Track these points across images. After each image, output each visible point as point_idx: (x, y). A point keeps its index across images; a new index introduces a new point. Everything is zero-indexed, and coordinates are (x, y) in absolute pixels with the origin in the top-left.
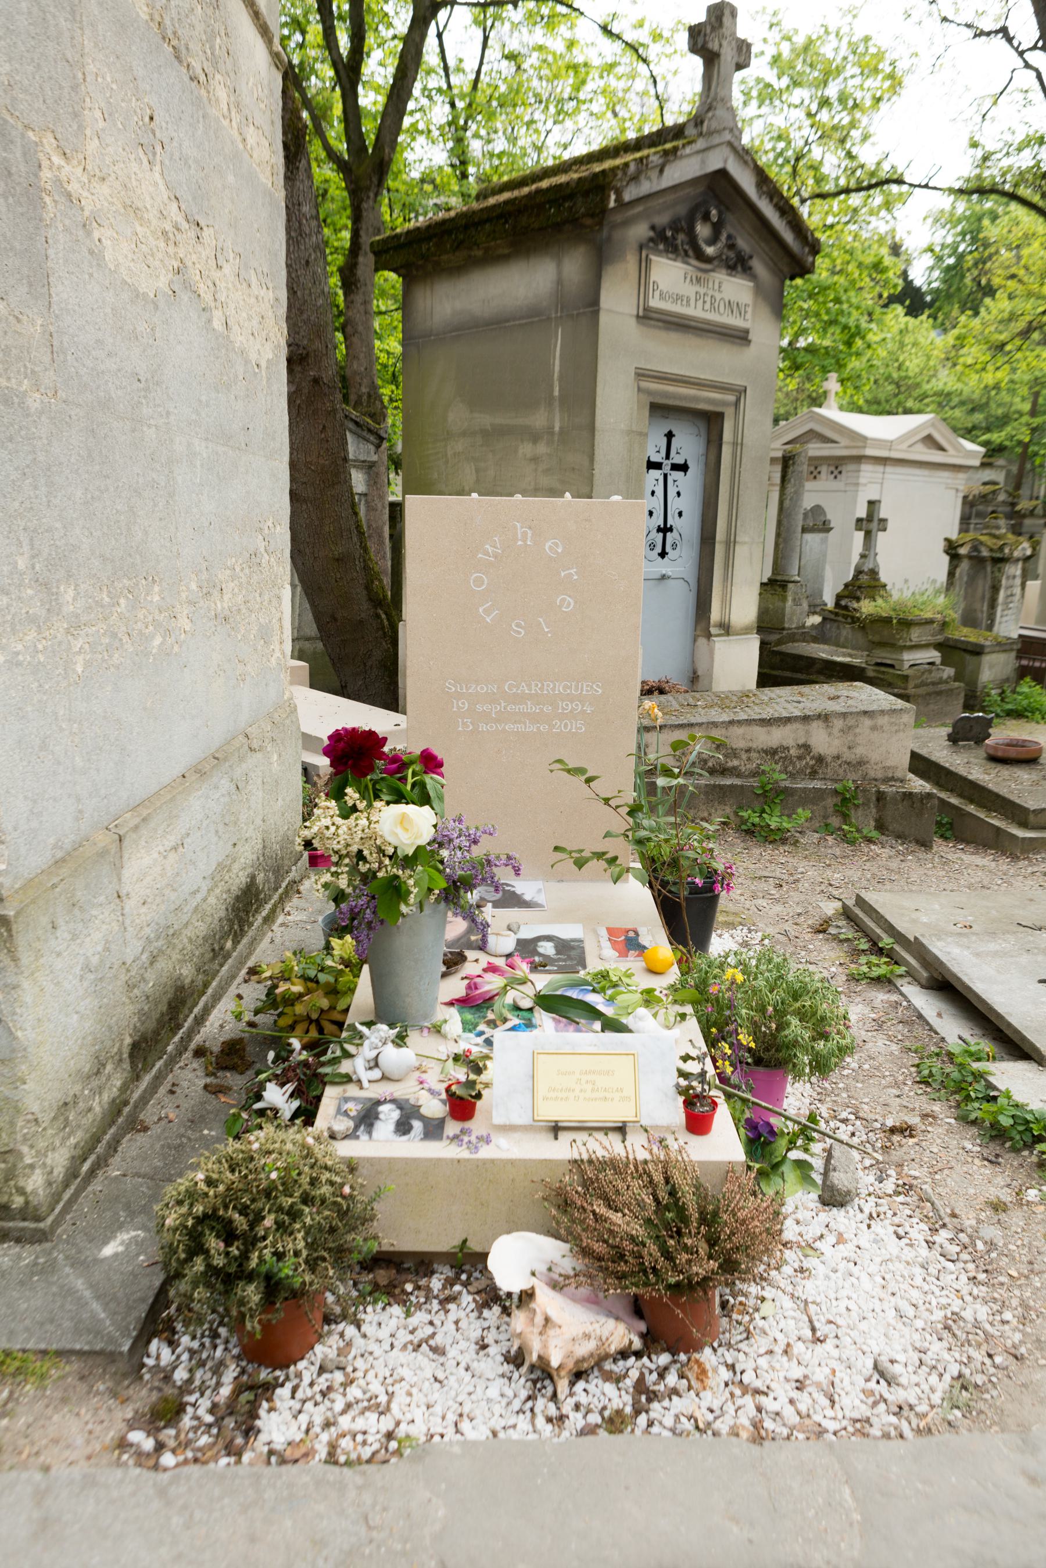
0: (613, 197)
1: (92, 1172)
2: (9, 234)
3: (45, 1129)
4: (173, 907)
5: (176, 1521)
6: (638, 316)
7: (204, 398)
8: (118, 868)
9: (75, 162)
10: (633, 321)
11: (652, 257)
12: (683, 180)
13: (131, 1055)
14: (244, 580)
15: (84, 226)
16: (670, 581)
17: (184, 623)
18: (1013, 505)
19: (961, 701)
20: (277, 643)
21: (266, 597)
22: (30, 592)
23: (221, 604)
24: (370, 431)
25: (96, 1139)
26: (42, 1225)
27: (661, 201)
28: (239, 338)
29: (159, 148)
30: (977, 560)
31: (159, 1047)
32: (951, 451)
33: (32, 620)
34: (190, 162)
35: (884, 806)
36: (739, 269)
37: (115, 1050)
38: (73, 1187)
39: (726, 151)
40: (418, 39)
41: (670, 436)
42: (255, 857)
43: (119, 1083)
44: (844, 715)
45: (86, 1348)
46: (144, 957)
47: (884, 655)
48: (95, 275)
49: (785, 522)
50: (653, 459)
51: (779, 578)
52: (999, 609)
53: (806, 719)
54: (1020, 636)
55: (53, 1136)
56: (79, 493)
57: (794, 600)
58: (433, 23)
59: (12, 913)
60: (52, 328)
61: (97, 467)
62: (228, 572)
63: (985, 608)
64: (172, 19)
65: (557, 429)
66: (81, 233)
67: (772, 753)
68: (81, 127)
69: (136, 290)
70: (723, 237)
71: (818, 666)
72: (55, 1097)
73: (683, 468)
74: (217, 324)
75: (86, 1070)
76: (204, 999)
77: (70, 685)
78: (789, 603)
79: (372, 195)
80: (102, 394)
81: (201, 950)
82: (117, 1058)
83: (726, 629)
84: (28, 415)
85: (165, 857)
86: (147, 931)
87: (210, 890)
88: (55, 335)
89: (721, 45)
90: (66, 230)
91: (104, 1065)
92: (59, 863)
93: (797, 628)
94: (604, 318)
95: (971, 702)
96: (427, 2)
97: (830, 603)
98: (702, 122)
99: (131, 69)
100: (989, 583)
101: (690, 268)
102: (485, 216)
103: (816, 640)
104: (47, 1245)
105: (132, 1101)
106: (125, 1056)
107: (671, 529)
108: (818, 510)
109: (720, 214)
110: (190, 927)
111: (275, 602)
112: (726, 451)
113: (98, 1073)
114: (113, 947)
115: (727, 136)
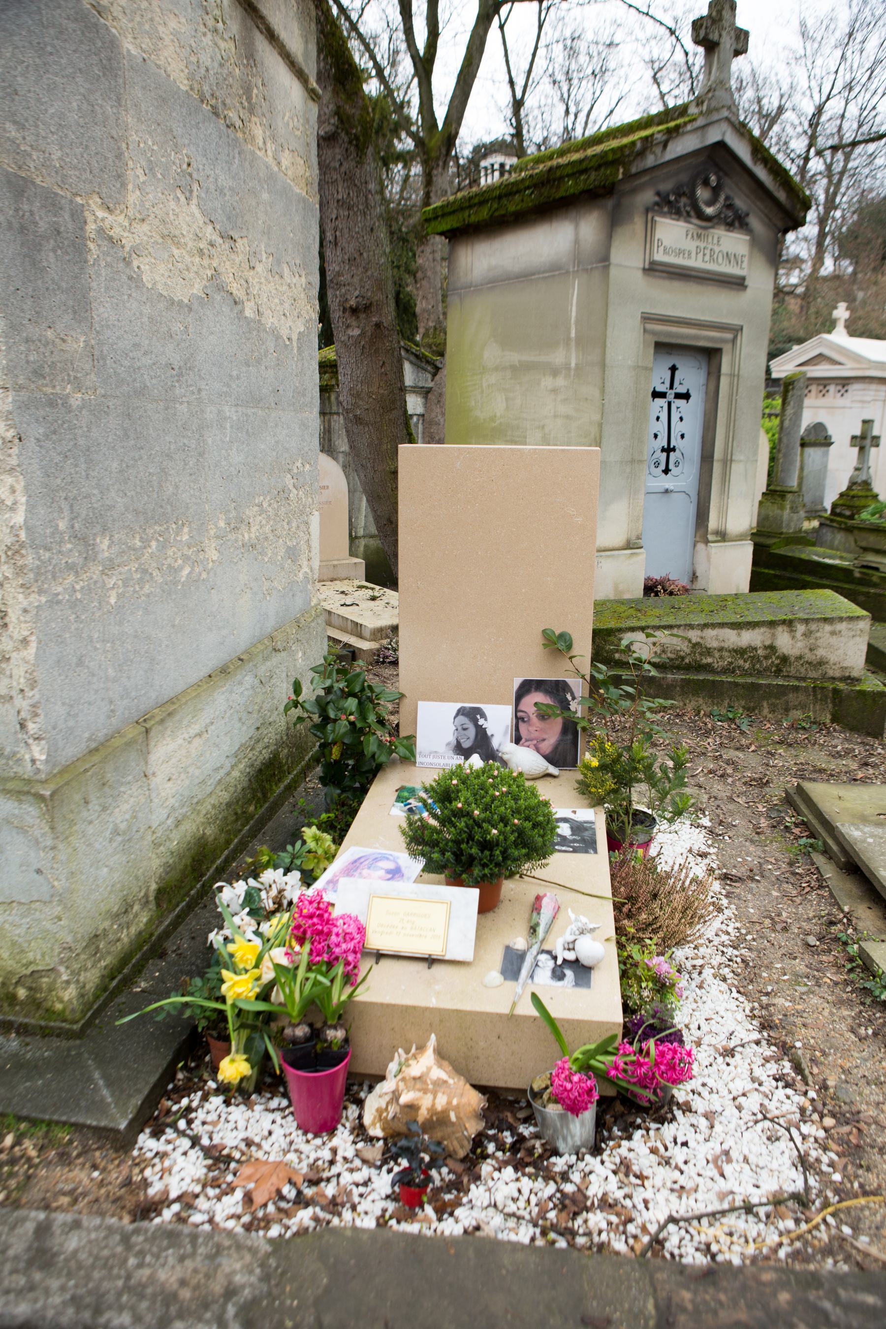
0: (621, 170)
2: (56, 278)
3: (78, 955)
4: (197, 781)
6: (644, 269)
7: (234, 373)
8: (145, 753)
10: (640, 273)
11: (657, 219)
12: (685, 152)
13: (157, 898)
14: (271, 512)
16: (673, 494)
20: (305, 563)
21: (294, 524)
22: (69, 546)
24: (428, 362)
26: (75, 1027)
27: (665, 171)
33: (70, 567)
34: (226, 191)
36: (737, 224)
37: (142, 894)
39: (724, 126)
40: (482, 33)
41: (673, 369)
42: (278, 737)
44: (806, 621)
46: (169, 822)
48: (134, 295)
53: (772, 624)
55: (85, 960)
56: (115, 464)
57: (792, 508)
58: (496, 17)
60: (93, 342)
61: (133, 442)
62: (256, 508)
64: (211, 85)
65: (573, 365)
67: (740, 652)
68: (124, 185)
70: (722, 198)
73: (686, 396)
75: (115, 910)
77: (104, 614)
79: (441, 163)
81: (225, 814)
82: (144, 900)
83: (722, 536)
84: (70, 412)
85: (189, 742)
86: (172, 801)
87: (232, 767)
89: (720, 36)
90: (108, 265)
91: (132, 907)
93: (795, 532)
94: (613, 271)
96: (491, 2)
98: (702, 102)
99: (171, 131)
101: (691, 226)
102: (515, 189)
106: (151, 898)
107: (674, 450)
108: (819, 428)
109: (719, 179)
110: (214, 796)
111: (303, 528)
112: (724, 382)
113: (126, 912)
114: (140, 815)
115: (725, 113)
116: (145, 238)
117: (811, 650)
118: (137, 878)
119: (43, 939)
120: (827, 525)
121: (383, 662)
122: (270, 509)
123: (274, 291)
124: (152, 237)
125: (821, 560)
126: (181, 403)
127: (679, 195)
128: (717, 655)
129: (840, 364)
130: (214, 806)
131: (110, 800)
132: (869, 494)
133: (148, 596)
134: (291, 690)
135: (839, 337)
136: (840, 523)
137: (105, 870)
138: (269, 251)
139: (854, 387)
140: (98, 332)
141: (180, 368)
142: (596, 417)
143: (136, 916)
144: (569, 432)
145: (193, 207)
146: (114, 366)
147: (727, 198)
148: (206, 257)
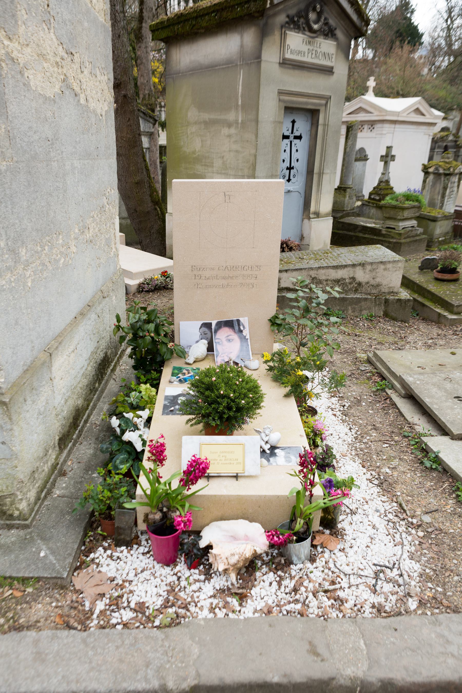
1: (45, 497)
5: (91, 653)
6: (280, 63)
7: (78, 140)
8: (50, 367)
9: (14, 40)
10: (277, 66)
11: (287, 32)
15: (21, 72)
16: (292, 193)
17: (74, 249)
18: (456, 141)
19: (425, 244)
22: (7, 256)
23: (88, 235)
25: (46, 482)
26: (26, 522)
28: (92, 105)
29: (52, 20)
30: (437, 175)
31: (70, 437)
32: (428, 116)
34: (67, 22)
35: (388, 305)
36: (330, 35)
38: (38, 504)
41: (293, 122)
43: (54, 457)
44: (372, 264)
45: (49, 576)
47: (391, 223)
48: (27, 95)
49: (347, 159)
50: (285, 134)
51: (343, 186)
52: (446, 198)
53: (354, 266)
54: (455, 210)
55: (29, 486)
56: (25, 204)
57: (349, 197)
59: (8, 400)
60: (9, 128)
63: (439, 198)
65: (240, 121)
66: (19, 76)
68: (16, 21)
69: (46, 97)
70: (322, 20)
71: (359, 229)
72: (28, 470)
73: (299, 138)
74: (82, 101)
76: (87, 412)
77: (26, 293)
78: (347, 198)
80: (33, 153)
81: (85, 391)
83: (318, 215)
85: (69, 356)
88: (10, 131)
90: (13, 77)
91: (48, 451)
92: (26, 371)
93: (350, 210)
94: (263, 65)
95: (430, 244)
97: (366, 197)
100: (442, 185)
102: (206, 12)
103: (359, 215)
104: (29, 530)
105: (60, 463)
106: (57, 444)
107: (293, 168)
109: (321, 7)
112: (320, 129)
113: (46, 455)
116: (30, 57)
117: (373, 278)
118: (50, 435)
119: (7, 478)
120: (366, 205)
121: (142, 291)
122: (97, 218)
123: (93, 86)
124: (32, 56)
125: (365, 225)
126: (54, 162)
127: (299, 17)
128: (325, 283)
129: (371, 113)
130: (81, 388)
131: (36, 396)
132: (389, 187)
133: (45, 278)
134: (115, 320)
135: (370, 97)
136: (373, 203)
137: (36, 435)
138: (90, 61)
139: (377, 126)
140: (11, 122)
141: (52, 140)
142: (253, 151)
143: (50, 455)
144: (238, 160)
145: (52, 34)
146: (20, 142)
147: (326, 19)
148: (60, 67)
